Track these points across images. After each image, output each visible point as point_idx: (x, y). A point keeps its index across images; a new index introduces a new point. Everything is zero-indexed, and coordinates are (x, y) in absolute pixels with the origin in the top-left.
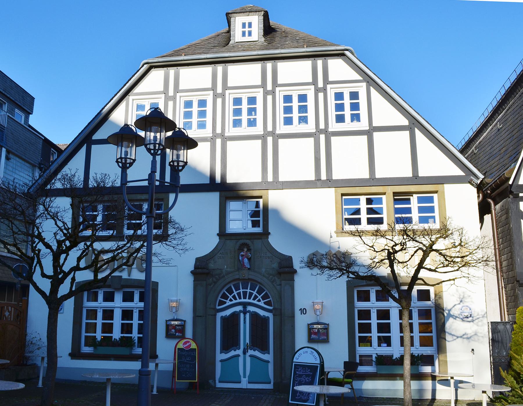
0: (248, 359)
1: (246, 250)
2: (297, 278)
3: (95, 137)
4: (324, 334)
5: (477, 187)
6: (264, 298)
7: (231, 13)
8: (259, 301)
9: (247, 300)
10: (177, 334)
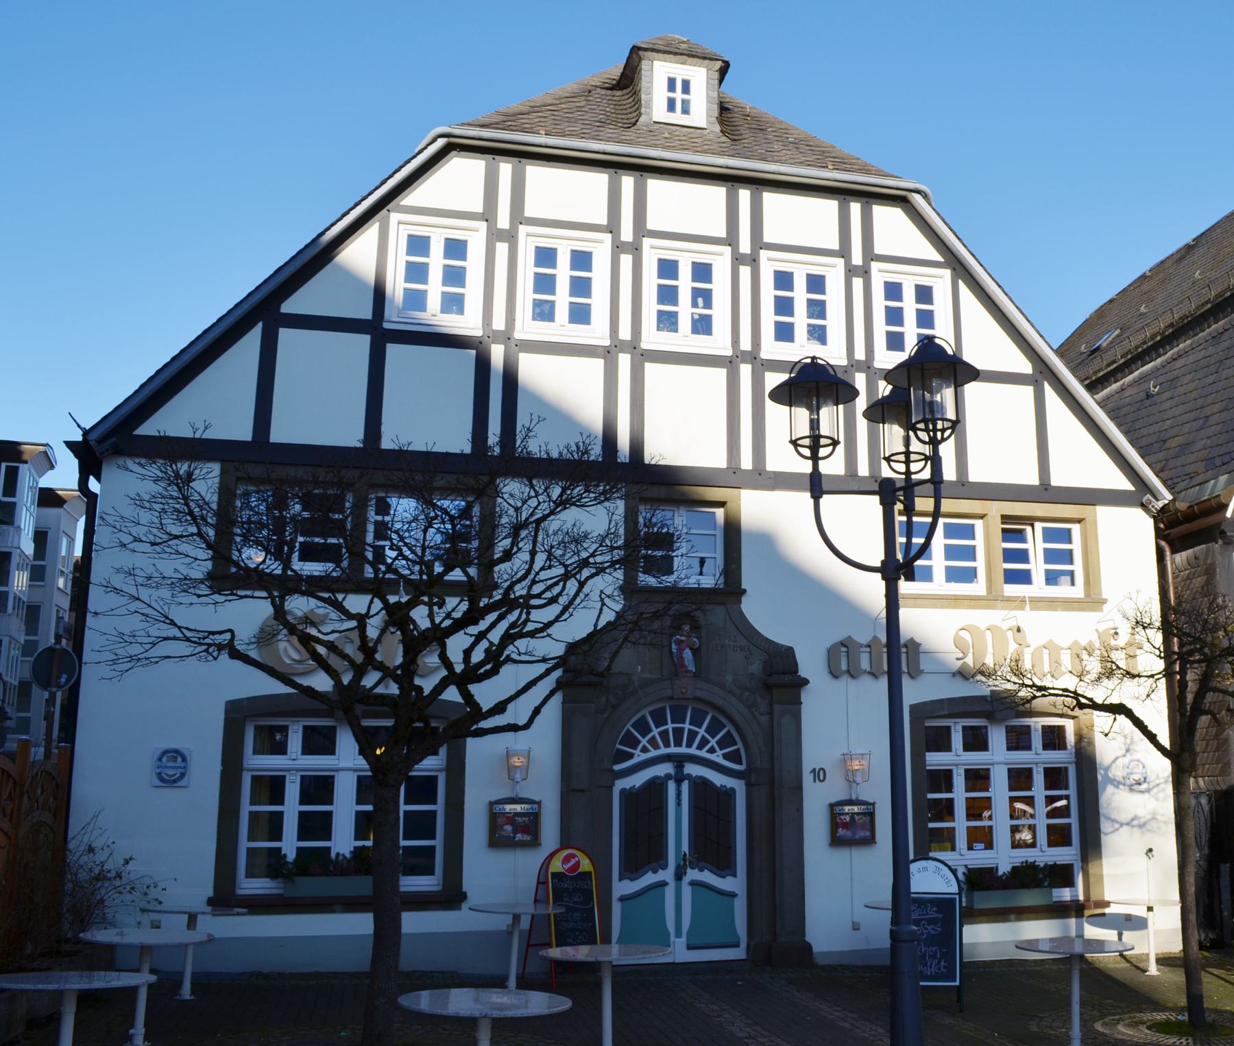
0: (687, 891)
1: (687, 628)
2: (806, 697)
3: (288, 307)
4: (863, 827)
5: (1154, 517)
6: (722, 744)
7: (646, 50)
8: (712, 751)
9: (683, 750)
10: (519, 836)
